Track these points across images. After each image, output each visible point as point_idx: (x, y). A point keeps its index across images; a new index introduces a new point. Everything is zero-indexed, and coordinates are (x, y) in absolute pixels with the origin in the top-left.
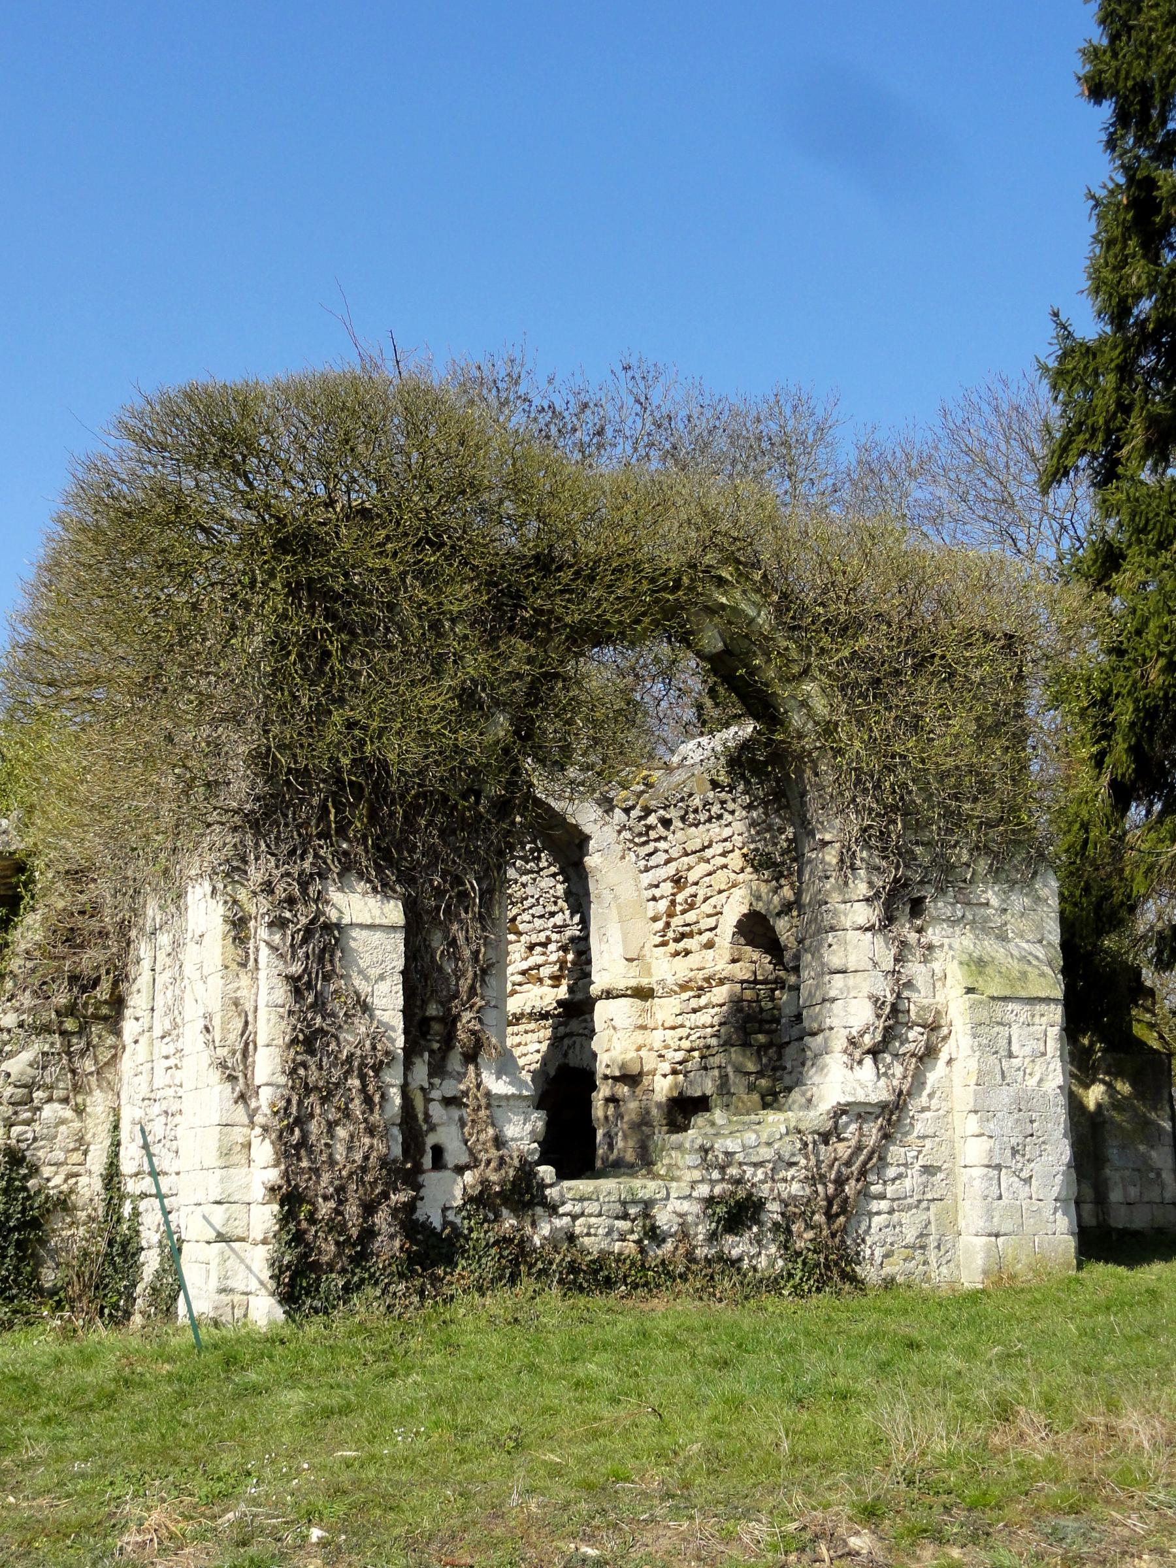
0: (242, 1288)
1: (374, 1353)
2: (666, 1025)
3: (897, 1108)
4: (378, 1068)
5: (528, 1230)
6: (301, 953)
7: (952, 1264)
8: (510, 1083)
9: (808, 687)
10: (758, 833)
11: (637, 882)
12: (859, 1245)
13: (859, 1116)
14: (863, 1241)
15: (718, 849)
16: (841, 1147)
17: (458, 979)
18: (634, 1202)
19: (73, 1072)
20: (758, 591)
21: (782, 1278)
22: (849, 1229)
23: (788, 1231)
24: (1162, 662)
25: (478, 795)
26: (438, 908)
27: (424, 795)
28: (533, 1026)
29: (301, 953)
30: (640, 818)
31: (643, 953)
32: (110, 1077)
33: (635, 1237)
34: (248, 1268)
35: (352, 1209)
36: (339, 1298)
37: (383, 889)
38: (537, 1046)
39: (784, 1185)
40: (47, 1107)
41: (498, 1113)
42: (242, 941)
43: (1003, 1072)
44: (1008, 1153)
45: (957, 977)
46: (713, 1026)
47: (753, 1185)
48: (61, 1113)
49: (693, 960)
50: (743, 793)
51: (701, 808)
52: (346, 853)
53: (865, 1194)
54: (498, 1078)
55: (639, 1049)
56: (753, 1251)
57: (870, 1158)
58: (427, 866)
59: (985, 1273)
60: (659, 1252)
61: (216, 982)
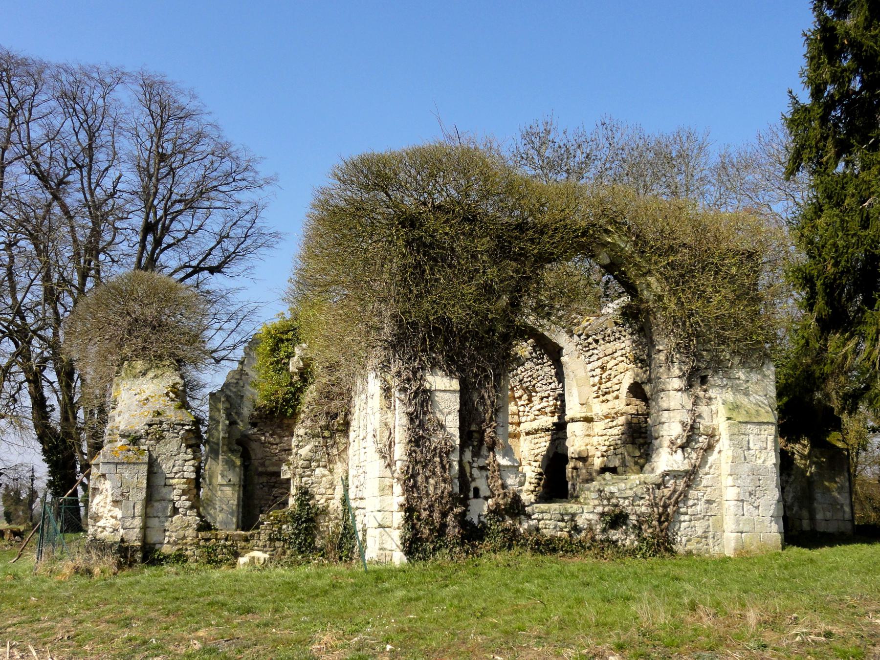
0: (389, 548)
1: (441, 577)
4: (447, 453)
5: (518, 526)
6: (413, 402)
7: (720, 546)
9: (651, 279)
10: (636, 346)
11: (585, 369)
13: (675, 476)
14: (677, 534)
15: (619, 353)
16: (666, 490)
17: (485, 414)
18: (567, 514)
19: (328, 454)
20: (625, 235)
23: (640, 529)
24: (832, 261)
25: (493, 331)
26: (475, 382)
27: (469, 332)
28: (543, 434)
29: (413, 402)
30: (585, 339)
32: (344, 456)
33: (567, 530)
34: (392, 539)
35: (436, 515)
36: (431, 553)
37: (450, 374)
38: (545, 444)
40: (317, 469)
41: (503, 473)
42: (388, 398)
43: (745, 457)
44: (747, 494)
45: (723, 412)
46: (618, 435)
47: (623, 507)
48: (323, 472)
49: (610, 404)
50: (629, 327)
52: (434, 359)
53: (677, 512)
54: (504, 458)
55: (587, 445)
56: (623, 537)
57: (680, 496)
58: (471, 364)
59: (735, 550)
60: (579, 537)
61: (378, 416)
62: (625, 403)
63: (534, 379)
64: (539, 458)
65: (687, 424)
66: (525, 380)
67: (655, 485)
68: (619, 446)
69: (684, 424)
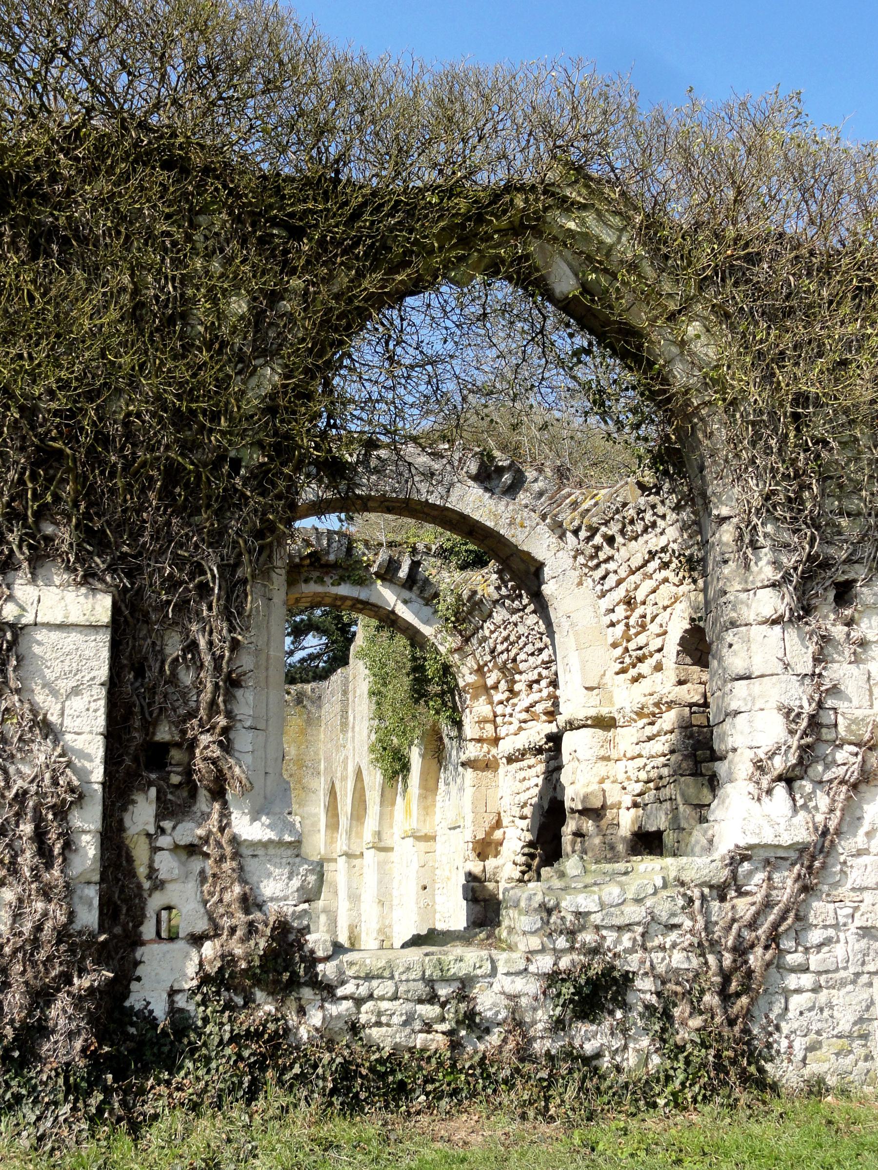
2: (629, 755)
3: (821, 851)
4: (61, 812)
8: (268, 826)
10: (690, 537)
12: (770, 1034)
13: (767, 862)
14: (778, 1028)
16: (742, 904)
21: (658, 1080)
22: (756, 1013)
23: (667, 1016)
30: (589, 539)
31: (604, 681)
33: (445, 1027)
39: (661, 955)
41: (251, 865)
47: (616, 955)
49: (644, 686)
51: (636, 517)
53: (776, 965)
54: (254, 819)
55: (601, 782)
56: (617, 1044)
57: (783, 918)
60: (481, 1047)
62: (674, 679)
63: (512, 644)
64: (528, 811)
65: (799, 715)
66: (500, 648)
67: (711, 887)
68: (665, 781)
69: (790, 714)
